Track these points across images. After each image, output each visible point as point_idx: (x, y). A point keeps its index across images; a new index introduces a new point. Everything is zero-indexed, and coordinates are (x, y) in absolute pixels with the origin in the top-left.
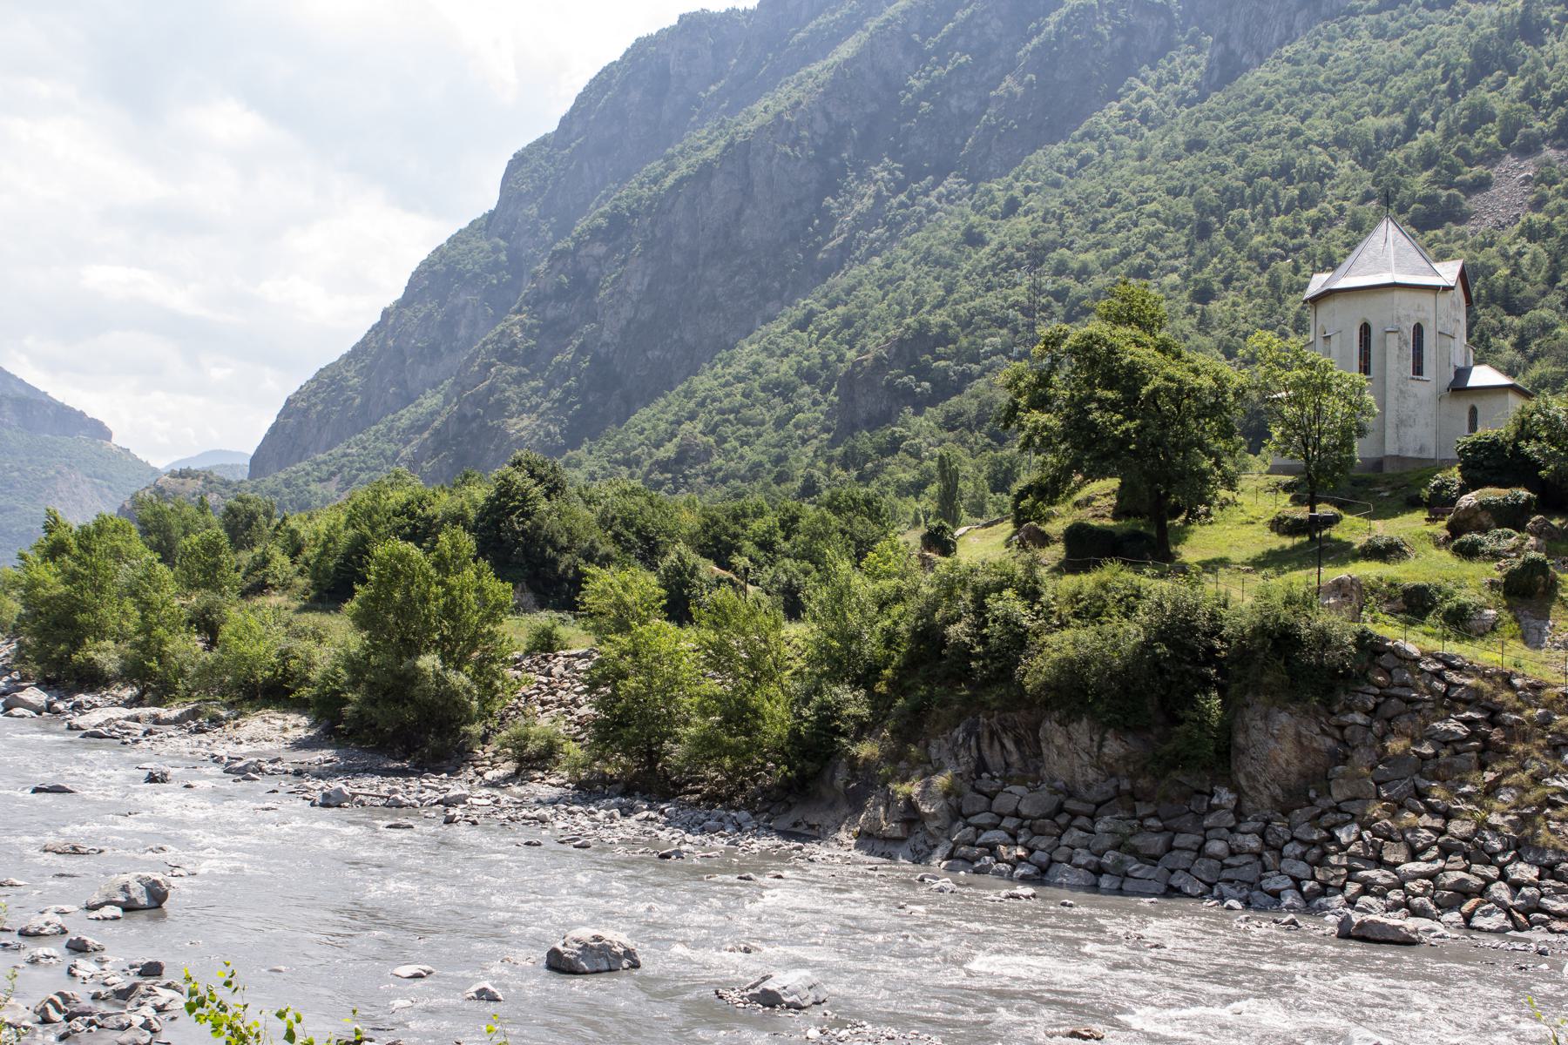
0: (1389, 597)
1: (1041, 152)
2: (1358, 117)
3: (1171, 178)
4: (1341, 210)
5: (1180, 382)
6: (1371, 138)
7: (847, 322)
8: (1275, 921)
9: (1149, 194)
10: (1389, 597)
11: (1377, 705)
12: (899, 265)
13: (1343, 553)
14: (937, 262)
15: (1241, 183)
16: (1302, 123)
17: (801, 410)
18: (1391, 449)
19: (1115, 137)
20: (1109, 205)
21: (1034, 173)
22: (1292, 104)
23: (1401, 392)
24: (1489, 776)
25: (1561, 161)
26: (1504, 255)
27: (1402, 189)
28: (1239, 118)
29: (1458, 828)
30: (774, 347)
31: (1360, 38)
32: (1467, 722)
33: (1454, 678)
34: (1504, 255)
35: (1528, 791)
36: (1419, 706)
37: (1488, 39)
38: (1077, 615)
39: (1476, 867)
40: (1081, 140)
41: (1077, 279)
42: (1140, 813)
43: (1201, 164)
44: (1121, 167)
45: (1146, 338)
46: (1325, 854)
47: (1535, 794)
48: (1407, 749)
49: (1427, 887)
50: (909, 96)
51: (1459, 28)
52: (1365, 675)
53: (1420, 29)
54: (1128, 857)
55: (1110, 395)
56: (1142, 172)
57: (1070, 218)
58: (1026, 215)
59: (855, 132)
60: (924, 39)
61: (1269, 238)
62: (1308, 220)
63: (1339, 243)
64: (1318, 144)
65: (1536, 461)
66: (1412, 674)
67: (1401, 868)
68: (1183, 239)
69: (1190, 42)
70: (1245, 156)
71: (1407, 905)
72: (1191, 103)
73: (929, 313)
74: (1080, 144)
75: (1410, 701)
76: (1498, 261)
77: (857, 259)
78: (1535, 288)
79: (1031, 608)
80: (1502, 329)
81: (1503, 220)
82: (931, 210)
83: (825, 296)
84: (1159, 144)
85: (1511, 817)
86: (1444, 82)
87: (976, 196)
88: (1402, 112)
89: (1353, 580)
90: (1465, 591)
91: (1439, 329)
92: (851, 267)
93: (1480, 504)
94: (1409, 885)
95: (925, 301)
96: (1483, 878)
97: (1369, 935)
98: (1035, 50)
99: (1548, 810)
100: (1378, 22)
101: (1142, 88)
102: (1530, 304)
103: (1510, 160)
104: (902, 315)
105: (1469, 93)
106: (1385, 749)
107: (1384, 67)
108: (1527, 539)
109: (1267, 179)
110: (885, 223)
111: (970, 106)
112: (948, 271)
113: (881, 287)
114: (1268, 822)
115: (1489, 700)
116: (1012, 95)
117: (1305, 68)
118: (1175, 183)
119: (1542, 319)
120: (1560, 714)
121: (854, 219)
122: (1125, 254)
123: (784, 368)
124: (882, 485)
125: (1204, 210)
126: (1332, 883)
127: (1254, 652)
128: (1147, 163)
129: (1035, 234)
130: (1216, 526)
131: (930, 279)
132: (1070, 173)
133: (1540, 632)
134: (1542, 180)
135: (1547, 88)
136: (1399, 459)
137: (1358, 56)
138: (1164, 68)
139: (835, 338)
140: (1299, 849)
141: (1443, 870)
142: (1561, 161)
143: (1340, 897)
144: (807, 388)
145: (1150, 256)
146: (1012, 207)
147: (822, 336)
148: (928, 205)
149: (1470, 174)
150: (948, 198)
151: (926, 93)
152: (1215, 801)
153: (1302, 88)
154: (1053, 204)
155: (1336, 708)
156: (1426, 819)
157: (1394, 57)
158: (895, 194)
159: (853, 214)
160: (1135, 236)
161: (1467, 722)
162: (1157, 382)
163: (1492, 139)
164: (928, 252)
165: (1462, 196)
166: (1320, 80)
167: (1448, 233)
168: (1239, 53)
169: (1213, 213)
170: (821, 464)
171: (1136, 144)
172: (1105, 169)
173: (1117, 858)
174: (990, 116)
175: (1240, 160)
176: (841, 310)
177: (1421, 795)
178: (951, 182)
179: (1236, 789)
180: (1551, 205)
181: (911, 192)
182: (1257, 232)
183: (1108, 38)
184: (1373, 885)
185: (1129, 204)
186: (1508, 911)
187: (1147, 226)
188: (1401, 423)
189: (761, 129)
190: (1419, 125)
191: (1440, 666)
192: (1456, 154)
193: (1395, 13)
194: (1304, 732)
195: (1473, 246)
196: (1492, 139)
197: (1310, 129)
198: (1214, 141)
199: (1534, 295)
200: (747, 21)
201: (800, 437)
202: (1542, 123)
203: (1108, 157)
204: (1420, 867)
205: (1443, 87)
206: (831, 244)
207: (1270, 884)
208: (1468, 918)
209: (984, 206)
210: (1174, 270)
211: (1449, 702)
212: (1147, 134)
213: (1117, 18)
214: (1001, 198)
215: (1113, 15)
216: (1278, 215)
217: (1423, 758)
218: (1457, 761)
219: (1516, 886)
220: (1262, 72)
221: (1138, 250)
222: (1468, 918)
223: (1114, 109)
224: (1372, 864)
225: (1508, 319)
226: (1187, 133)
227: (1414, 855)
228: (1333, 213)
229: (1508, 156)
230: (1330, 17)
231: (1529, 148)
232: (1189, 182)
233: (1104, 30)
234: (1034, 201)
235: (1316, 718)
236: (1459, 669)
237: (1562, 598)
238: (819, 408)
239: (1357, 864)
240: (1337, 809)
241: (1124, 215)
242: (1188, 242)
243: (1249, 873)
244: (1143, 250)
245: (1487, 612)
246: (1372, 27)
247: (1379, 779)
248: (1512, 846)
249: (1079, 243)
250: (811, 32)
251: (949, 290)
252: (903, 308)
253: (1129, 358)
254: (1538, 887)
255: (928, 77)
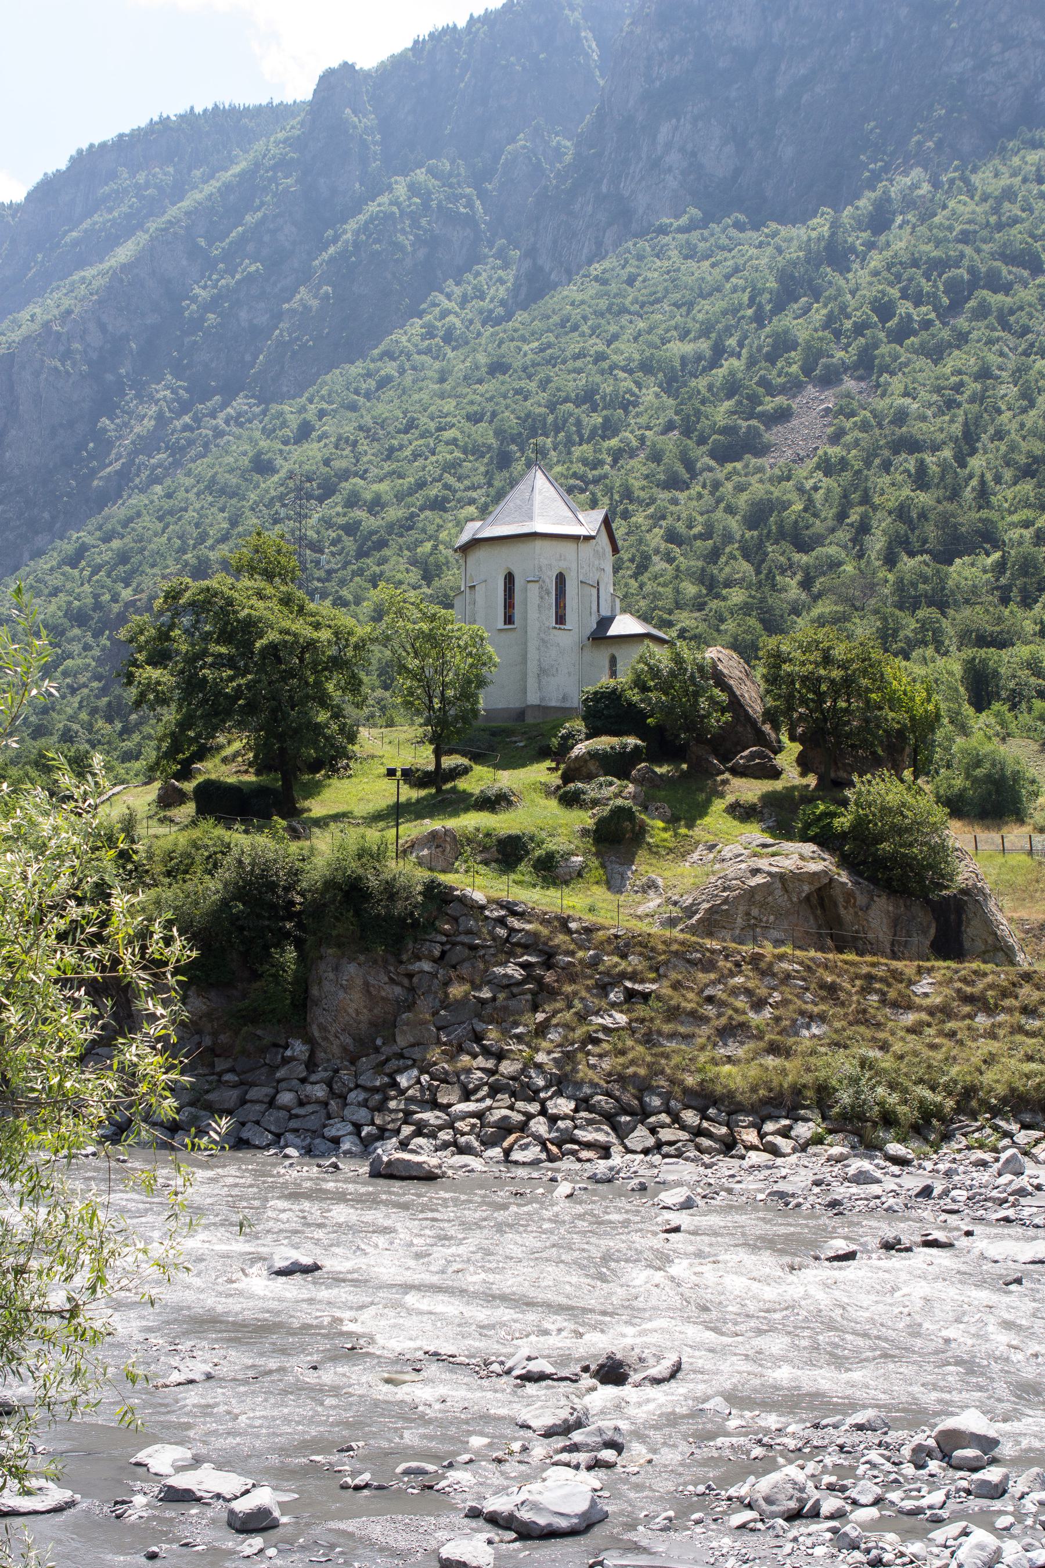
0: (485, 848)
1: (338, 371)
2: (664, 341)
3: (472, 403)
4: (642, 439)
5: (295, 635)
6: (677, 364)
7: (123, 558)
8: (319, 1166)
9: (448, 419)
10: (485, 848)
11: (443, 953)
12: (181, 494)
13: (463, 803)
14: (222, 492)
15: (543, 410)
16: (608, 346)
17: (70, 656)
18: (533, 699)
19: (416, 356)
20: (406, 432)
21: (329, 395)
22: (599, 326)
23: (543, 641)
24: (540, 1017)
25: (860, 392)
26: (800, 489)
27: (703, 419)
28: (544, 340)
29: (507, 1067)
30: (42, 586)
31: (669, 258)
32: (524, 966)
33: (515, 923)
34: (800, 489)
35: (573, 1030)
36: (482, 952)
37: (794, 264)
38: (168, 874)
39: (520, 1105)
40: (381, 359)
41: (370, 511)
42: (218, 1069)
43: (503, 389)
44: (421, 389)
45: (269, 591)
46: (387, 1099)
47: (580, 1032)
48: (467, 994)
49: (474, 1126)
50: (194, 307)
51: (770, 250)
52: (433, 924)
53: (730, 251)
54: (203, 1113)
55: (223, 650)
56: (442, 396)
57: (364, 446)
58: (319, 440)
59: (134, 346)
60: (210, 244)
61: (568, 469)
62: (609, 450)
63: (638, 475)
64: (624, 369)
65: (642, 710)
66: (476, 921)
67: (453, 1109)
68: (482, 469)
69: (496, 257)
70: (548, 380)
71: (455, 1144)
72: (498, 322)
73: (212, 548)
74: (379, 364)
75: (473, 948)
76: (793, 496)
77: (136, 487)
78: (825, 524)
79: (124, 868)
80: (791, 566)
81: (802, 453)
82: (219, 434)
83: (100, 528)
84: (461, 366)
85: (556, 1055)
86: (750, 307)
87: (267, 419)
88: (709, 338)
89: (446, 831)
90: (556, 840)
91: (581, 578)
92: (130, 496)
93: (589, 753)
94: (459, 1125)
95: (207, 534)
96: (525, 1114)
97: (395, 1172)
98: (332, 260)
99: (590, 1047)
100: (688, 242)
101: (447, 304)
102: (818, 540)
103: (811, 390)
104: (182, 550)
105: (775, 319)
106: (447, 995)
107: (692, 289)
108: (626, 787)
109: (570, 406)
110: (167, 448)
111: (262, 320)
112: (234, 501)
113: (160, 519)
114: (336, 1071)
115: (545, 944)
116: (307, 308)
117: (613, 287)
118: (475, 408)
119: (829, 557)
120: (608, 955)
121: (133, 443)
122: (421, 485)
123: (52, 608)
124: (143, 738)
125: (504, 438)
126: (389, 1127)
127: (324, 905)
128: (447, 386)
129: (327, 462)
130: (353, 779)
131: (214, 510)
132: (368, 396)
133: (623, 877)
134: (841, 411)
135: (848, 317)
136: (539, 708)
137: (666, 277)
138: (469, 283)
139: (109, 576)
140: (362, 1096)
141: (490, 1108)
142: (860, 392)
143: (394, 1140)
144: (76, 631)
145: (447, 487)
146: (305, 432)
147: (94, 573)
148: (215, 429)
149: (770, 404)
150: (237, 420)
151: (213, 304)
152: (288, 1053)
153: (609, 309)
154: (347, 429)
155: (404, 957)
156: (481, 1061)
157: (703, 279)
158: (179, 415)
159: (132, 437)
160: (431, 465)
161: (524, 966)
162: (272, 636)
163: (794, 369)
164: (213, 480)
165: (762, 427)
166: (627, 302)
167: (746, 466)
168: (547, 269)
169: (513, 441)
170: (84, 716)
171: (437, 365)
172: (404, 393)
173: (190, 1113)
174: (283, 330)
175: (544, 384)
176: (116, 544)
177: (478, 1038)
178: (240, 403)
179: (310, 1041)
180: (848, 439)
181: (196, 414)
182: (558, 462)
183: (409, 249)
184: (425, 1126)
185: (427, 431)
186: (543, 1143)
187: (445, 454)
188: (543, 672)
189: (27, 339)
190: (725, 352)
191: (503, 913)
192: (758, 384)
193: (706, 233)
194: (372, 981)
195: (771, 480)
196: (794, 369)
197: (616, 353)
198: (517, 364)
199: (822, 531)
200: (13, 216)
201: (69, 686)
202: (842, 354)
203: (409, 377)
204: (471, 1106)
205: (750, 312)
206: (108, 470)
207: (331, 1132)
208: (507, 1152)
209: (274, 430)
210: (472, 502)
211: (508, 948)
212: (451, 354)
213: (419, 228)
214: (294, 422)
215: (415, 224)
216: (580, 445)
217: (483, 1002)
218: (511, 1003)
219: (553, 1119)
220: (571, 291)
221: (435, 480)
222: (507, 1152)
223: (416, 327)
224: (429, 1106)
225: (797, 557)
226: (489, 355)
227: (467, 1095)
228: (635, 443)
229: (810, 387)
230: (640, 235)
231: (829, 379)
232: (489, 407)
233: (406, 241)
234: (328, 426)
235: (385, 967)
236: (520, 915)
237: (648, 844)
238: (90, 653)
239: (413, 1108)
240: (401, 1056)
241: (421, 442)
242: (487, 472)
243: (313, 1122)
244: (439, 481)
245: (574, 859)
246: (682, 247)
247: (439, 1024)
248: (554, 1082)
249: (374, 471)
250: (86, 231)
251: (234, 523)
252: (184, 542)
253: (246, 611)
254: (573, 1119)
255: (215, 286)
